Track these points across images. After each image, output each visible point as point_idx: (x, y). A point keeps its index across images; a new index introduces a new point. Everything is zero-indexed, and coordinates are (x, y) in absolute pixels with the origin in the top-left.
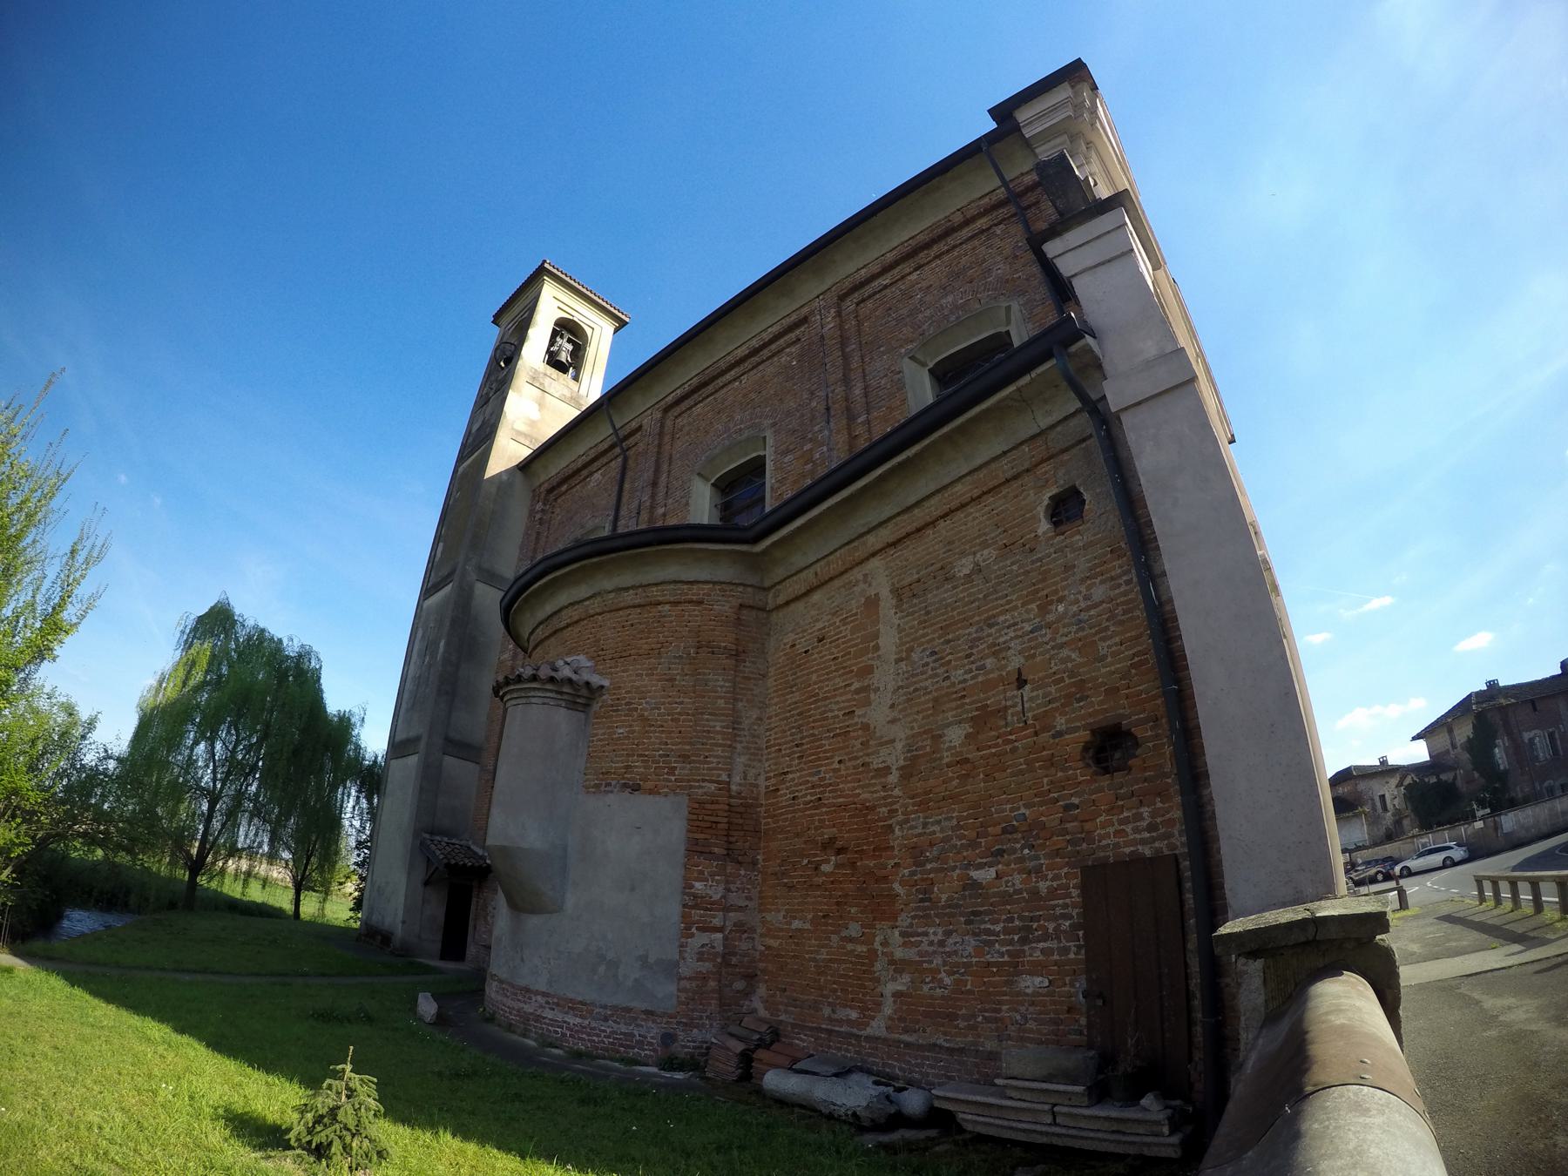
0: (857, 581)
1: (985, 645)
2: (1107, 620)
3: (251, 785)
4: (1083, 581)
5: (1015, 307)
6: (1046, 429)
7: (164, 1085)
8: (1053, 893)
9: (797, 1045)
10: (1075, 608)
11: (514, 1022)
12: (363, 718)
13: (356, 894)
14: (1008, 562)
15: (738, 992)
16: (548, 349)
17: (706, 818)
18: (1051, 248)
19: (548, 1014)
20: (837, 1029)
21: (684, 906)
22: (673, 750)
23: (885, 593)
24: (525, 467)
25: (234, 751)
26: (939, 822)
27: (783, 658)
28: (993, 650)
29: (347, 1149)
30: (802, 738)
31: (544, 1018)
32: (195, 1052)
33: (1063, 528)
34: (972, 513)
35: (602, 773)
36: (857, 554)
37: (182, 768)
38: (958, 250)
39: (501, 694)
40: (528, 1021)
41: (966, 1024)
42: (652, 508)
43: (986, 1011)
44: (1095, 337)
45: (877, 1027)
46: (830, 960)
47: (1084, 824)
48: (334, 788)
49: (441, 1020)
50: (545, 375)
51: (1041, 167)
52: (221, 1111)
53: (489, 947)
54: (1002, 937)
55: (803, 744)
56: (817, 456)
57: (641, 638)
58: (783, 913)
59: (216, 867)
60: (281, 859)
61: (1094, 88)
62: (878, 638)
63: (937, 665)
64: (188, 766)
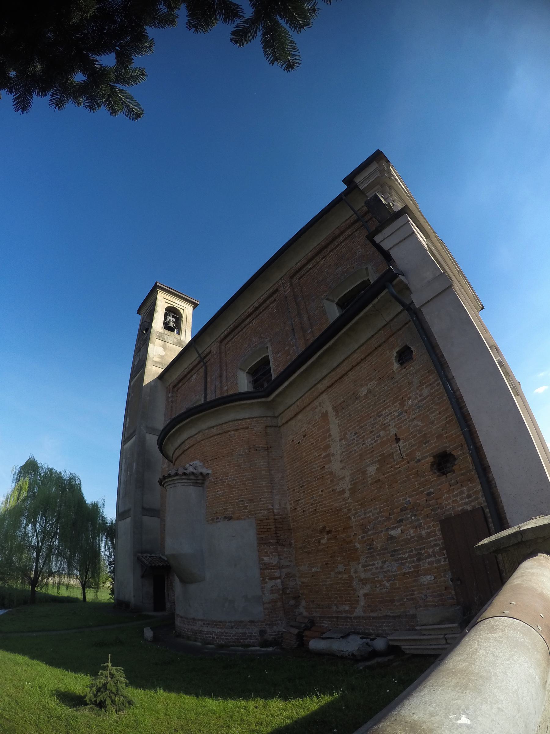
0: (317, 406)
1: (378, 426)
2: (432, 404)
3: (55, 541)
4: (417, 388)
5: (370, 267)
6: (390, 321)
7: (27, 683)
8: (428, 534)
9: (323, 626)
10: (416, 401)
11: (190, 635)
12: (104, 504)
13: (112, 586)
14: (383, 386)
15: (292, 606)
16: (164, 322)
17: (265, 527)
18: (378, 239)
19: (205, 629)
20: (340, 615)
21: (261, 569)
22: (245, 498)
23: (330, 409)
24: (161, 377)
25: (45, 527)
26: (371, 511)
27: (289, 447)
28: (382, 427)
29: (113, 702)
30: (303, 483)
31: (203, 631)
32: (41, 667)
33: (405, 365)
34: (363, 366)
35: (214, 514)
36: (314, 394)
37: (22, 538)
38: (340, 246)
39: (162, 484)
40: (197, 634)
41: (399, 603)
42: (221, 387)
43: (407, 596)
44: (403, 275)
45: (359, 612)
46: (332, 584)
47: (438, 500)
48: (94, 538)
49: (156, 639)
50: (164, 334)
51: (367, 203)
52: (54, 692)
53: (174, 603)
54: (409, 560)
55: (304, 486)
56: (292, 352)
57: (223, 449)
58: (307, 566)
59: (44, 582)
60: (74, 574)
61: (388, 161)
62: (330, 431)
63: (358, 439)
64: (24, 536)
